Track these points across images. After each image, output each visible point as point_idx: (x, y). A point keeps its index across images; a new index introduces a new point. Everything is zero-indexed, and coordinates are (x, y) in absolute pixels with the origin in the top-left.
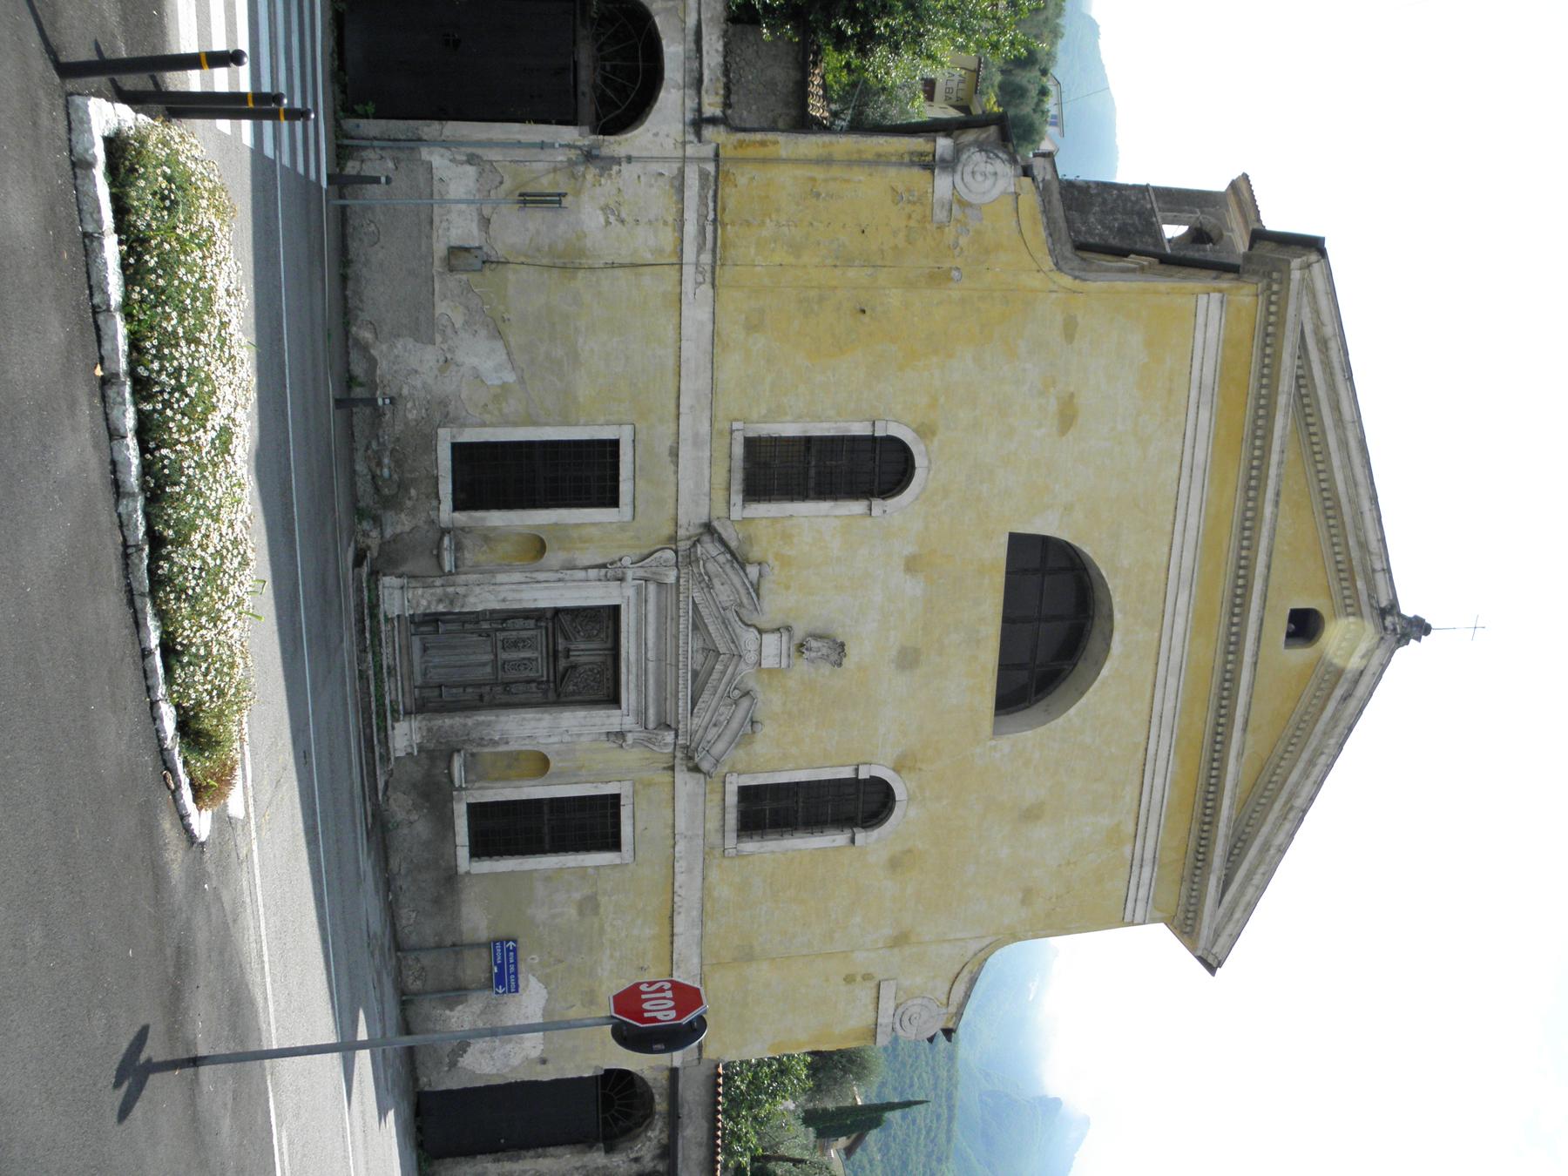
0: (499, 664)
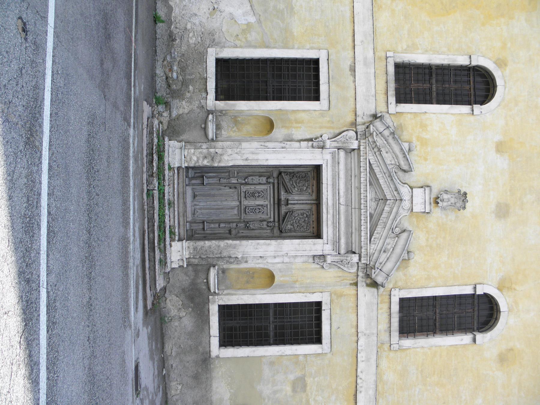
0: (243, 208)
